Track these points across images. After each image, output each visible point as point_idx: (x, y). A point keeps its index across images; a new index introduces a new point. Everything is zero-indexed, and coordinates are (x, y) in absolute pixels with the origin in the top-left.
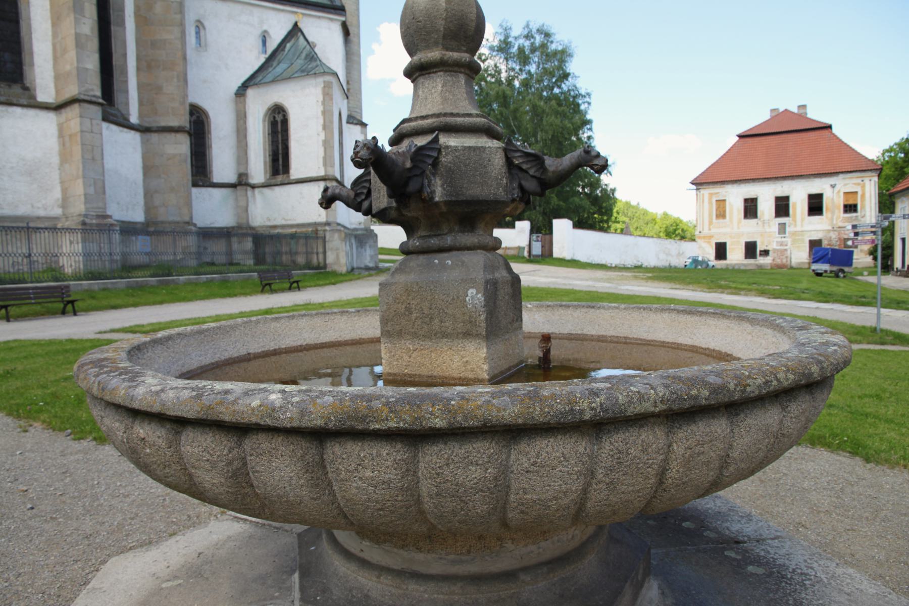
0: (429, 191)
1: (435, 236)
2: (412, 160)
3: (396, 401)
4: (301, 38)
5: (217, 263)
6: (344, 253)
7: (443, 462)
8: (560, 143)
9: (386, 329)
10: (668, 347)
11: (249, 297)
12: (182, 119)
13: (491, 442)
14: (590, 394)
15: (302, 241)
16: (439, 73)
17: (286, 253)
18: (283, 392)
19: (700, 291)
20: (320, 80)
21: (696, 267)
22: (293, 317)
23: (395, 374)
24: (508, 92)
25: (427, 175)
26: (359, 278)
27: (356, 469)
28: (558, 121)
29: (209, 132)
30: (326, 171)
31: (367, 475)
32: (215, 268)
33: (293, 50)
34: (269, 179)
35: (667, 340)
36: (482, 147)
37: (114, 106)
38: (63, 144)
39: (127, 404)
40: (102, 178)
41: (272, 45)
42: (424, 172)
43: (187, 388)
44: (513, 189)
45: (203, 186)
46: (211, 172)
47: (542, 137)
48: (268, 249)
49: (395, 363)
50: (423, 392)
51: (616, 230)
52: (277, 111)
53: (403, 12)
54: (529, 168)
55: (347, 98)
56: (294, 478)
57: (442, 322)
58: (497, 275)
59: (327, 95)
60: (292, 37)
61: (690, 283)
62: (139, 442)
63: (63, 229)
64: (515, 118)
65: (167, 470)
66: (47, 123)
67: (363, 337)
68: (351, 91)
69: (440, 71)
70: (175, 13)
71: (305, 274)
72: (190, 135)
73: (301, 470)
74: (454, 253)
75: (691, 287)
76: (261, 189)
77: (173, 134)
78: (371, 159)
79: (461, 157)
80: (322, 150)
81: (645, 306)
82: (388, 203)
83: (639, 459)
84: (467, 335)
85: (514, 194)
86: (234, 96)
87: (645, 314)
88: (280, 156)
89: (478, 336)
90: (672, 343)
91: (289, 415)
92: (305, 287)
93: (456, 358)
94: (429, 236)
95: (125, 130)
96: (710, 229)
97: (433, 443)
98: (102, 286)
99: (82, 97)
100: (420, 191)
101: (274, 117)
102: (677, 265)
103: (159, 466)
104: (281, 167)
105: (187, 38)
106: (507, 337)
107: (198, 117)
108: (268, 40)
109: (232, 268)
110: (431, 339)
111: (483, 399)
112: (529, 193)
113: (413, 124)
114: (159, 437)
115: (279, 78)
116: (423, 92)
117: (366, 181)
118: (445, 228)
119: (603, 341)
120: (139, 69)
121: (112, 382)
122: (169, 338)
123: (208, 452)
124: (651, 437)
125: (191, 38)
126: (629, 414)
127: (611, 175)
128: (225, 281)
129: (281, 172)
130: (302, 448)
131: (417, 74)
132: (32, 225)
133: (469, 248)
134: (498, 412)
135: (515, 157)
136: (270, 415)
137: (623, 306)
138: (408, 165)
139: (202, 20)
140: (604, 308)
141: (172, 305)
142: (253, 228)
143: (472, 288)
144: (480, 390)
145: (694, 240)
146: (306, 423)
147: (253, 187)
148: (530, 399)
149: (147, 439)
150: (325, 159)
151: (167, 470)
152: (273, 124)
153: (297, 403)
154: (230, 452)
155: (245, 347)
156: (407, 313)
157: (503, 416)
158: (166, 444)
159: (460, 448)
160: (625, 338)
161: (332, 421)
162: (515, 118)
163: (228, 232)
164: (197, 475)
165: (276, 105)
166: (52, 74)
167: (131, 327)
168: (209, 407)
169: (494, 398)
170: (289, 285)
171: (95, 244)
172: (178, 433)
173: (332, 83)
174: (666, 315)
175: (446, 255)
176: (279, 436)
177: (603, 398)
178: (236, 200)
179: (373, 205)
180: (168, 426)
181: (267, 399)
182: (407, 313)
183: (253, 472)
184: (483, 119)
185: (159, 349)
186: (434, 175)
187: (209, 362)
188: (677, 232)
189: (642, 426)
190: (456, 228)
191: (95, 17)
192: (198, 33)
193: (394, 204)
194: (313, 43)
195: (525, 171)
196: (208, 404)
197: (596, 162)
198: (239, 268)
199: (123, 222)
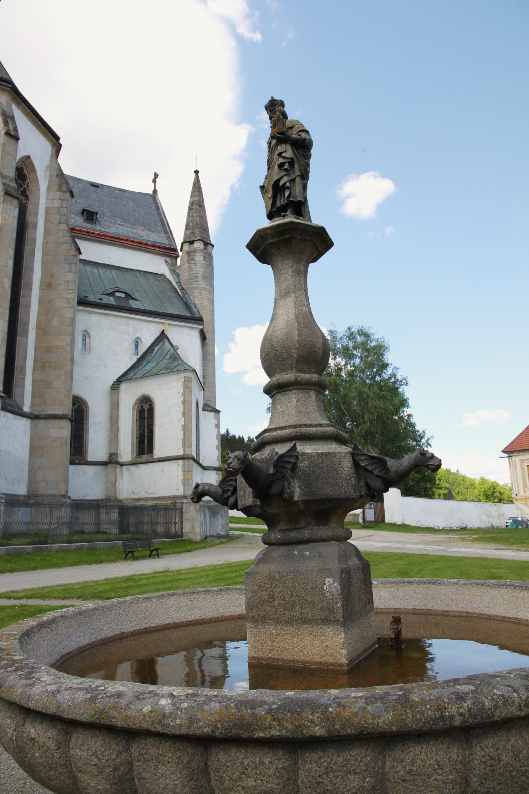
0: (289, 492)
1: (294, 529)
2: (275, 467)
3: (278, 709)
4: (167, 343)
5: (86, 531)
6: (199, 523)
7: (322, 770)
8: (384, 422)
9: (252, 614)
10: (510, 622)
11: (113, 563)
12: (66, 409)
13: (367, 750)
14: (457, 698)
15: (162, 512)
16: (293, 391)
17: (148, 523)
18: (171, 696)
19: (524, 551)
20: (181, 376)
21: (517, 527)
22: (162, 596)
23: (259, 658)
24: (338, 381)
25: (287, 478)
26: (211, 546)
27: (240, 778)
28: (381, 404)
29: (87, 419)
30: (184, 451)
31: (249, 784)
32: (85, 536)
33: (159, 352)
34: (136, 458)
35: (508, 615)
36: (333, 452)
37: (12, 398)
39: (23, 703)
41: (143, 349)
42: (284, 475)
43: (80, 689)
44: (361, 487)
45: (79, 464)
46: (86, 452)
47: (369, 418)
48: (132, 520)
49: (260, 647)
50: (301, 697)
51: (440, 495)
52: (145, 401)
53: (262, 342)
54: (373, 469)
55: (204, 390)
56: (179, 786)
57: (302, 609)
58: (350, 563)
59: (187, 388)
60: (160, 342)
61: (513, 543)
62: (28, 742)
64: (345, 402)
65: (52, 773)
67: (225, 615)
68: (207, 384)
69: (294, 389)
70: (68, 326)
71: (164, 543)
72: (71, 421)
73: (186, 778)
74: (312, 545)
75: (514, 547)
76: (128, 466)
77: (58, 421)
78: (241, 468)
79: (316, 462)
80: (181, 433)
81: (483, 581)
82: (253, 501)
83: (511, 766)
84: (326, 621)
85: (361, 492)
86: (110, 389)
87: (483, 589)
88: (146, 439)
89: (336, 622)
90: (512, 618)
91: (178, 722)
92: (164, 554)
93: (317, 643)
94: (289, 530)
95: (19, 417)
96: (525, 492)
97: (313, 750)
100: (282, 492)
101: (142, 406)
102: (499, 525)
103: (45, 767)
104: (146, 448)
105: (76, 344)
106: (361, 621)
107: (79, 406)
108: (140, 344)
109: (100, 536)
110: (293, 625)
111: (358, 705)
112: (374, 490)
113: (273, 434)
114: (49, 738)
115: (147, 374)
116: (281, 406)
117: (232, 480)
118: (303, 522)
119: (446, 616)
120: (34, 369)
121: (10, 679)
122: (53, 621)
123: (97, 757)
124: (520, 742)
125: (78, 344)
126: (496, 719)
127: (430, 446)
128: (92, 549)
129: (146, 452)
130: (188, 754)
131: (275, 392)
133: (324, 540)
134: (373, 719)
135: (362, 460)
136: (160, 722)
137: (462, 582)
138: (271, 471)
139: (88, 331)
140: (444, 584)
141: (44, 571)
142: (119, 501)
143: (329, 577)
144: (353, 694)
145: (512, 502)
146: (195, 730)
147: (122, 465)
148: (402, 705)
149: (37, 739)
150: (184, 441)
151: (52, 773)
152: (141, 412)
153: (186, 709)
154: (118, 757)
155: (119, 627)
156: (270, 600)
157: (378, 723)
158: (55, 746)
159: (338, 756)
160: (467, 613)
161: (218, 728)
162: (345, 402)
163: (98, 504)
164: (82, 780)
165: (144, 396)
167: (7, 593)
168: (103, 712)
169: (368, 705)
170: (150, 552)
172: (68, 734)
173: (191, 378)
174: (503, 591)
175: (304, 546)
176: (166, 741)
177: (469, 702)
178: (107, 475)
179: (239, 501)
180: (59, 727)
181: (157, 704)
182: (270, 600)
183: (139, 779)
184: (332, 428)
185: (45, 631)
186: (293, 477)
187: (87, 643)
188: (495, 495)
189: (509, 730)
190: (313, 522)
192: (84, 340)
193: (258, 503)
194: (176, 346)
195: (371, 472)
196: (102, 707)
197: (431, 462)
198: (106, 537)
199: (8, 495)
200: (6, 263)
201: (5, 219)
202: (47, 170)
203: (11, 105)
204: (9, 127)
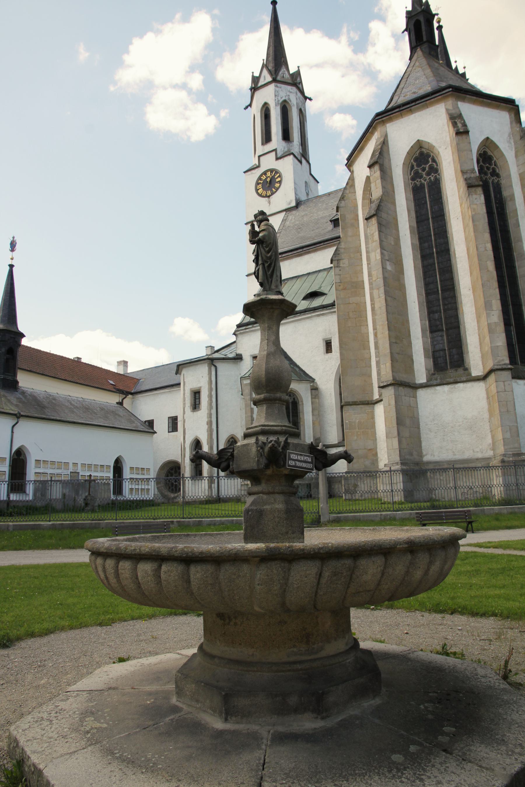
38: (489, 404)
40: (516, 424)
63: (493, 467)
66: (479, 388)
98: (510, 511)
99: (496, 367)
132: (456, 466)
166: (480, 355)
171: (512, 477)
191: (500, 308)
200: (485, 247)
201: (474, 209)
202: (510, 138)
203: (457, 105)
204: (458, 127)
